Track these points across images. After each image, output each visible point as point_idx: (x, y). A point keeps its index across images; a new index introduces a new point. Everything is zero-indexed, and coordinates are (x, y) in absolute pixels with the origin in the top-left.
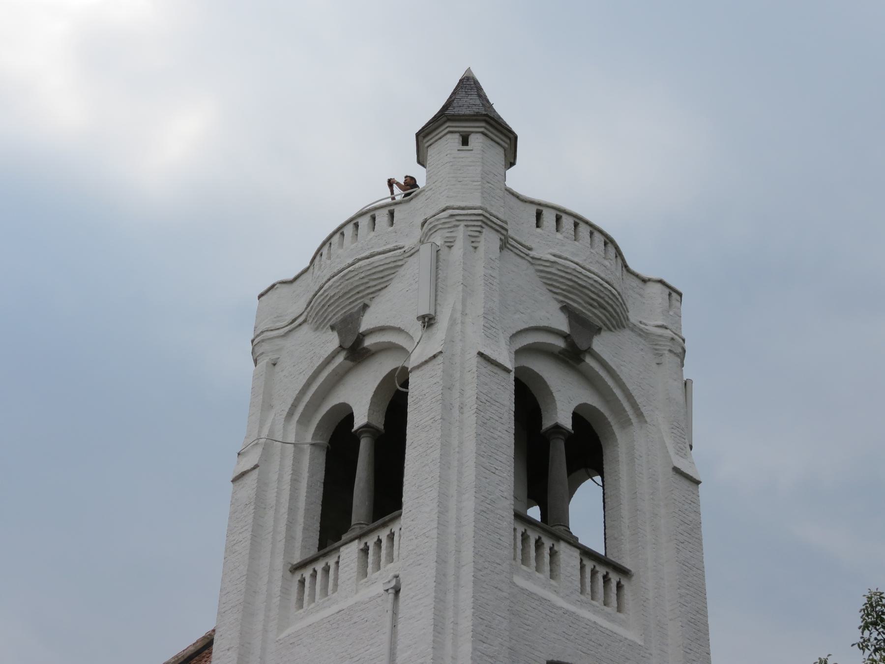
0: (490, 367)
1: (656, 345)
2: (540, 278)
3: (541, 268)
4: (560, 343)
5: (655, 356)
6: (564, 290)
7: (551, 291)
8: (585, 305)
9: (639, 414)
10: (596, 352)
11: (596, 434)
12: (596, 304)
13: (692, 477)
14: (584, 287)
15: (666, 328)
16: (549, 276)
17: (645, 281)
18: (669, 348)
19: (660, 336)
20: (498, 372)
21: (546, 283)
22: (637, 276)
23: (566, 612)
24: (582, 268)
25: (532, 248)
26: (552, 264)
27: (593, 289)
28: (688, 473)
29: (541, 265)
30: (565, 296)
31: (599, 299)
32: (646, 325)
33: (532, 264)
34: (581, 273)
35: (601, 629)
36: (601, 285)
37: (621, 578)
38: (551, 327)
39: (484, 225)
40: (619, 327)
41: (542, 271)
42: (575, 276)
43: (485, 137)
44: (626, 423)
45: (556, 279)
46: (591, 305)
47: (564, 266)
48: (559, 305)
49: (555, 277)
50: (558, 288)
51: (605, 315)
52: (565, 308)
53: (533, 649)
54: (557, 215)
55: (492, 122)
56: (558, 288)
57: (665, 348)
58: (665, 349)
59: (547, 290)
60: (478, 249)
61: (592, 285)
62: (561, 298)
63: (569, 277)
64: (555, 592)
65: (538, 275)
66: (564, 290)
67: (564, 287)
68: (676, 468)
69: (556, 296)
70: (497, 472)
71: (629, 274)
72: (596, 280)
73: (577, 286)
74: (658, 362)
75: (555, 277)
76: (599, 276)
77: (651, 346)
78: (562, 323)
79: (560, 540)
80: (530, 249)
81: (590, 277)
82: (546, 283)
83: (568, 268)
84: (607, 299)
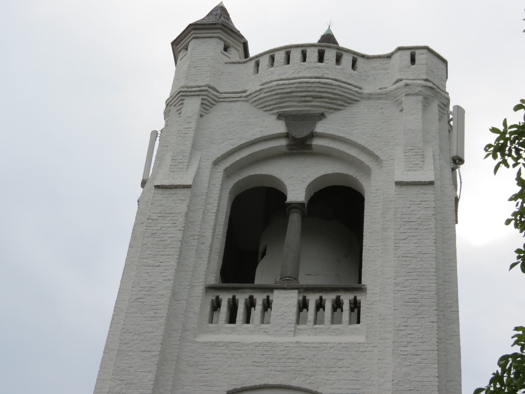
0: (168, 192)
1: (396, 97)
2: (255, 107)
3: (253, 99)
4: (283, 142)
5: (397, 107)
6: (276, 104)
7: (266, 111)
8: (299, 104)
9: (376, 158)
10: (320, 133)
11: (280, 192)
12: (308, 99)
13: (420, 182)
14: (291, 92)
15: (401, 80)
16: (260, 101)
17: (389, 57)
18: (404, 95)
19: (396, 89)
20: (177, 192)
21: (261, 108)
22: (379, 57)
23: (258, 345)
24: (288, 80)
25: (245, 90)
26: (260, 92)
27: (300, 90)
28: (419, 180)
29: (253, 97)
30: (279, 108)
31: (310, 94)
32: (386, 88)
33: (247, 101)
34: (284, 84)
35: (306, 345)
36: (307, 82)
37: (305, 295)
38: (264, 136)
39: (183, 98)
40: (214, 105)
41: (255, 101)
42: (280, 89)
43: (198, 39)
44: (367, 171)
45: (266, 100)
46: (306, 101)
47: (268, 88)
48: (275, 117)
49: (265, 100)
50: (271, 105)
51: (324, 102)
52: (280, 116)
53: (211, 386)
54: (353, 58)
55: (206, 26)
56: (271, 105)
57: (402, 96)
58: (402, 97)
59: (264, 112)
60: (203, 117)
61: (297, 87)
62: (276, 111)
63: (275, 92)
64: (265, 334)
65: (253, 106)
66: (276, 104)
67: (274, 102)
68: (398, 182)
69: (272, 112)
70: (162, 264)
71: (370, 60)
72: (300, 81)
73: (285, 95)
74: (400, 110)
75: (265, 100)
76: (305, 78)
77: (392, 101)
78: (280, 127)
79: (274, 290)
80: (245, 92)
81: (293, 82)
82: (261, 108)
83: (271, 87)
84: (318, 89)
